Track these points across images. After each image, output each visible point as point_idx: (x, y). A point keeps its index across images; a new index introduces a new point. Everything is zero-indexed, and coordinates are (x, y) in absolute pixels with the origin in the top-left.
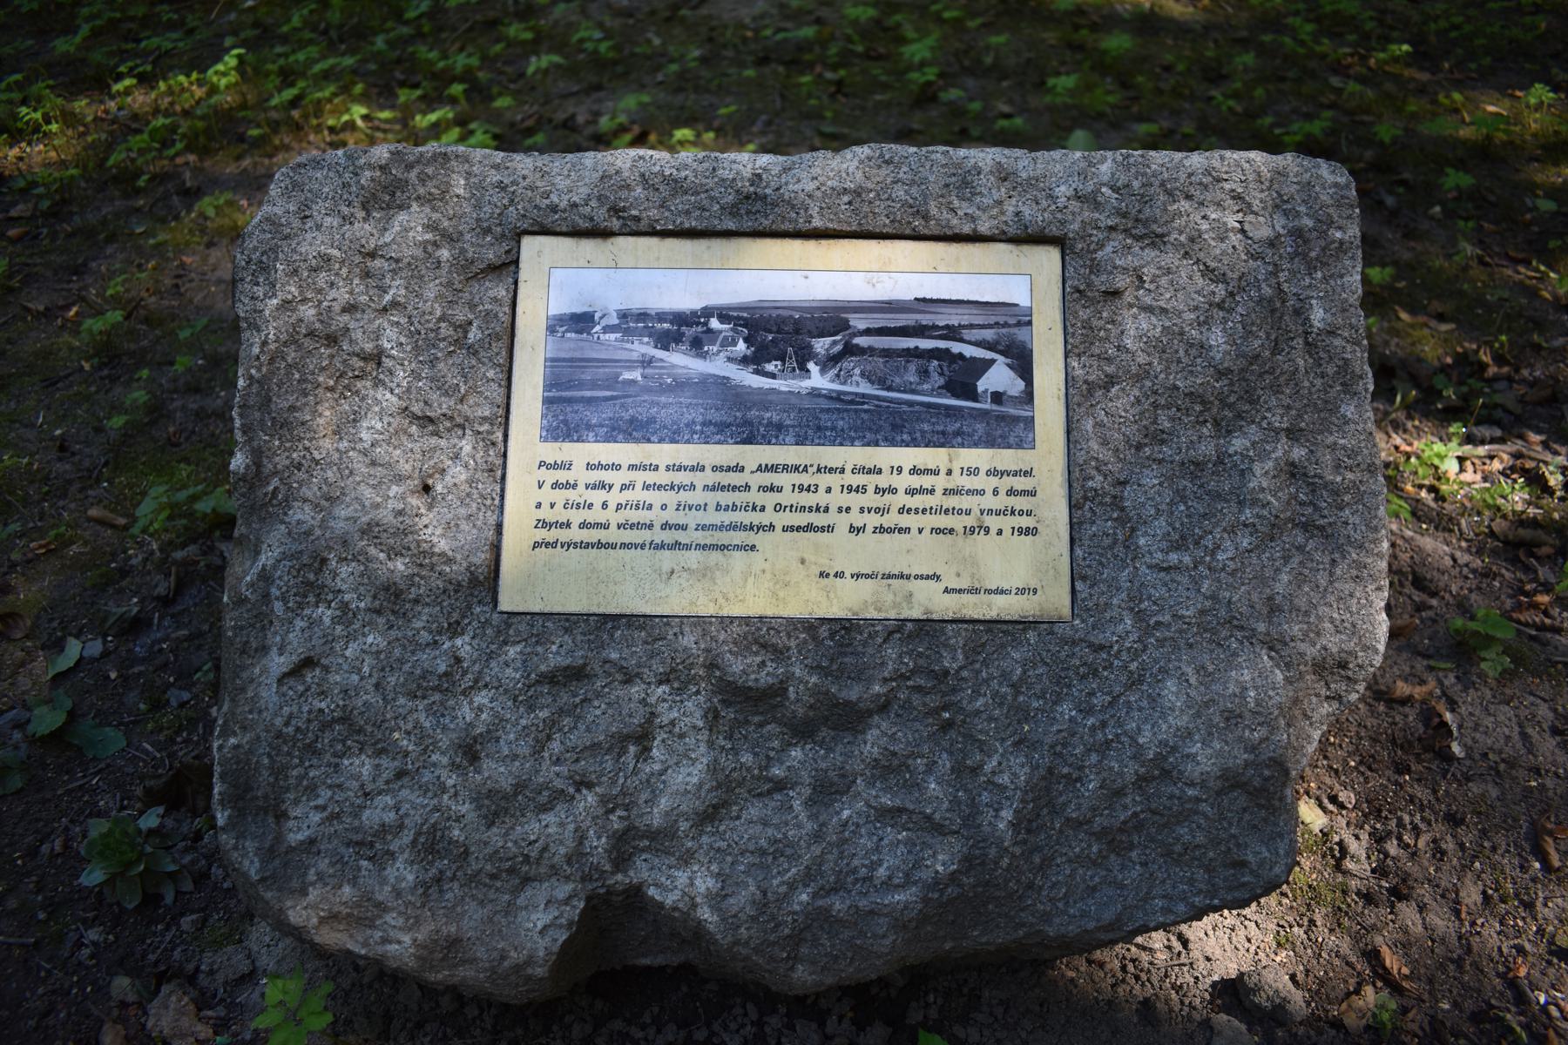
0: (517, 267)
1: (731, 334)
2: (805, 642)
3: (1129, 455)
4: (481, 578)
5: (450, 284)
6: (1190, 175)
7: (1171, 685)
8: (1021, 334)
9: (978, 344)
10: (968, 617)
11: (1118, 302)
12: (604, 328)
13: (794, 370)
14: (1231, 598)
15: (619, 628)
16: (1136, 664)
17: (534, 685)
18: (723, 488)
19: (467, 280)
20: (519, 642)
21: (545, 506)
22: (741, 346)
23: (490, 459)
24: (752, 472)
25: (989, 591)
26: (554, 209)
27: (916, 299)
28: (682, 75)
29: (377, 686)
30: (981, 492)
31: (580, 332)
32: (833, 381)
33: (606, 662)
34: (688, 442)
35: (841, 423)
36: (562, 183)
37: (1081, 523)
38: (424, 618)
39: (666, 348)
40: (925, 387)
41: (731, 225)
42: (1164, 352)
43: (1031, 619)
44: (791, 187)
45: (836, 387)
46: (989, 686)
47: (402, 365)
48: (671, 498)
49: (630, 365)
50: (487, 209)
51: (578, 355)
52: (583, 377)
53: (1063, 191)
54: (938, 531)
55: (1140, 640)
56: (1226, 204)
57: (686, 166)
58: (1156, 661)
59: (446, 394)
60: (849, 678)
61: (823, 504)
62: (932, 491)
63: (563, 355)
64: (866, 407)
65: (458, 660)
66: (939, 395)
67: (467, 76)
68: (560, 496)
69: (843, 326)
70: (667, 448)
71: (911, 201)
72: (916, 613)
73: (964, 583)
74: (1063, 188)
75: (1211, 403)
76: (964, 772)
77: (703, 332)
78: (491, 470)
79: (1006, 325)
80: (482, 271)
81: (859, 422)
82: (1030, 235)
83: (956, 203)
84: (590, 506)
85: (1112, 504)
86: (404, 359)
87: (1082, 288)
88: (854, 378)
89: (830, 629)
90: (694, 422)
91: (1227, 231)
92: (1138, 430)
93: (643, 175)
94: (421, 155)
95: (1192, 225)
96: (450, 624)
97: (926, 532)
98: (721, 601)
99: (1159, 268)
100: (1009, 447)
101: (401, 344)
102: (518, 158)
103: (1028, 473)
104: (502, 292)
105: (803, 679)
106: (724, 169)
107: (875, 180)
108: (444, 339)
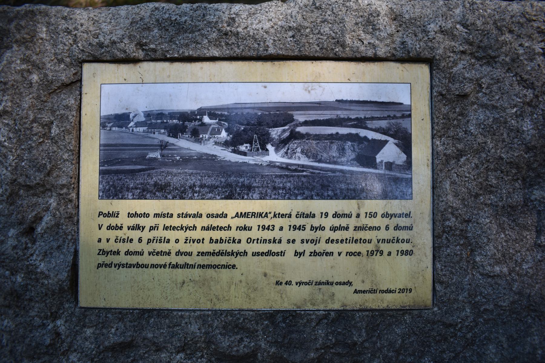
0: (81, 84)
1: (217, 126)
2: (267, 326)
3: (471, 201)
4: (66, 288)
5: (38, 97)
6: (512, 17)
7: (492, 348)
8: (404, 123)
9: (376, 130)
10: (369, 308)
11: (466, 101)
12: (136, 124)
13: (258, 149)
14: (530, 293)
15: (152, 317)
16: (470, 334)
17: (103, 352)
18: (214, 228)
19: (50, 94)
20: (92, 327)
21: (104, 241)
22: (224, 134)
23: (69, 211)
24: (232, 218)
25: (382, 292)
26: (101, 45)
27: (337, 101)
29: (11, 351)
30: (378, 228)
31: (120, 127)
32: (284, 157)
33: (144, 339)
34: (191, 198)
35: (289, 184)
36: (106, 28)
37: (440, 247)
38: (36, 310)
39: (175, 136)
40: (343, 159)
41: (216, 53)
42: (494, 135)
43: (408, 308)
44: (254, 26)
45: (286, 160)
46: (381, 352)
47: (11, 152)
48: (181, 235)
49: (152, 148)
50: (61, 46)
51: (120, 142)
52: (124, 156)
53: (432, 27)
54: (350, 254)
55: (474, 320)
56: (534, 37)
57: (185, 14)
58: (483, 333)
59: (39, 170)
60: (295, 347)
61: (277, 238)
62: (347, 228)
63: (111, 142)
64: (304, 173)
65: (58, 334)
66: (352, 165)
68: (112, 234)
69: (289, 120)
70: (178, 202)
71: (334, 35)
72: (336, 306)
73: (367, 287)
74: (432, 26)
75: (522, 168)
77: (199, 125)
78: (70, 217)
79: (395, 117)
80: (59, 88)
81: (300, 184)
82: (411, 57)
83: (363, 36)
84: (131, 241)
85: (460, 235)
86: (13, 148)
87: (444, 93)
88: (297, 154)
89: (283, 316)
90: (194, 185)
91: (535, 54)
92: (476, 185)
93: (157, 20)
94: (18, 12)
95: (513, 50)
96: (52, 313)
97: (343, 254)
98: (215, 300)
99: (492, 79)
100: (396, 198)
101: (10, 138)
102: (78, 12)
103: (408, 215)
104: (72, 102)
106: (210, 15)
107: (309, 21)
108: (36, 134)
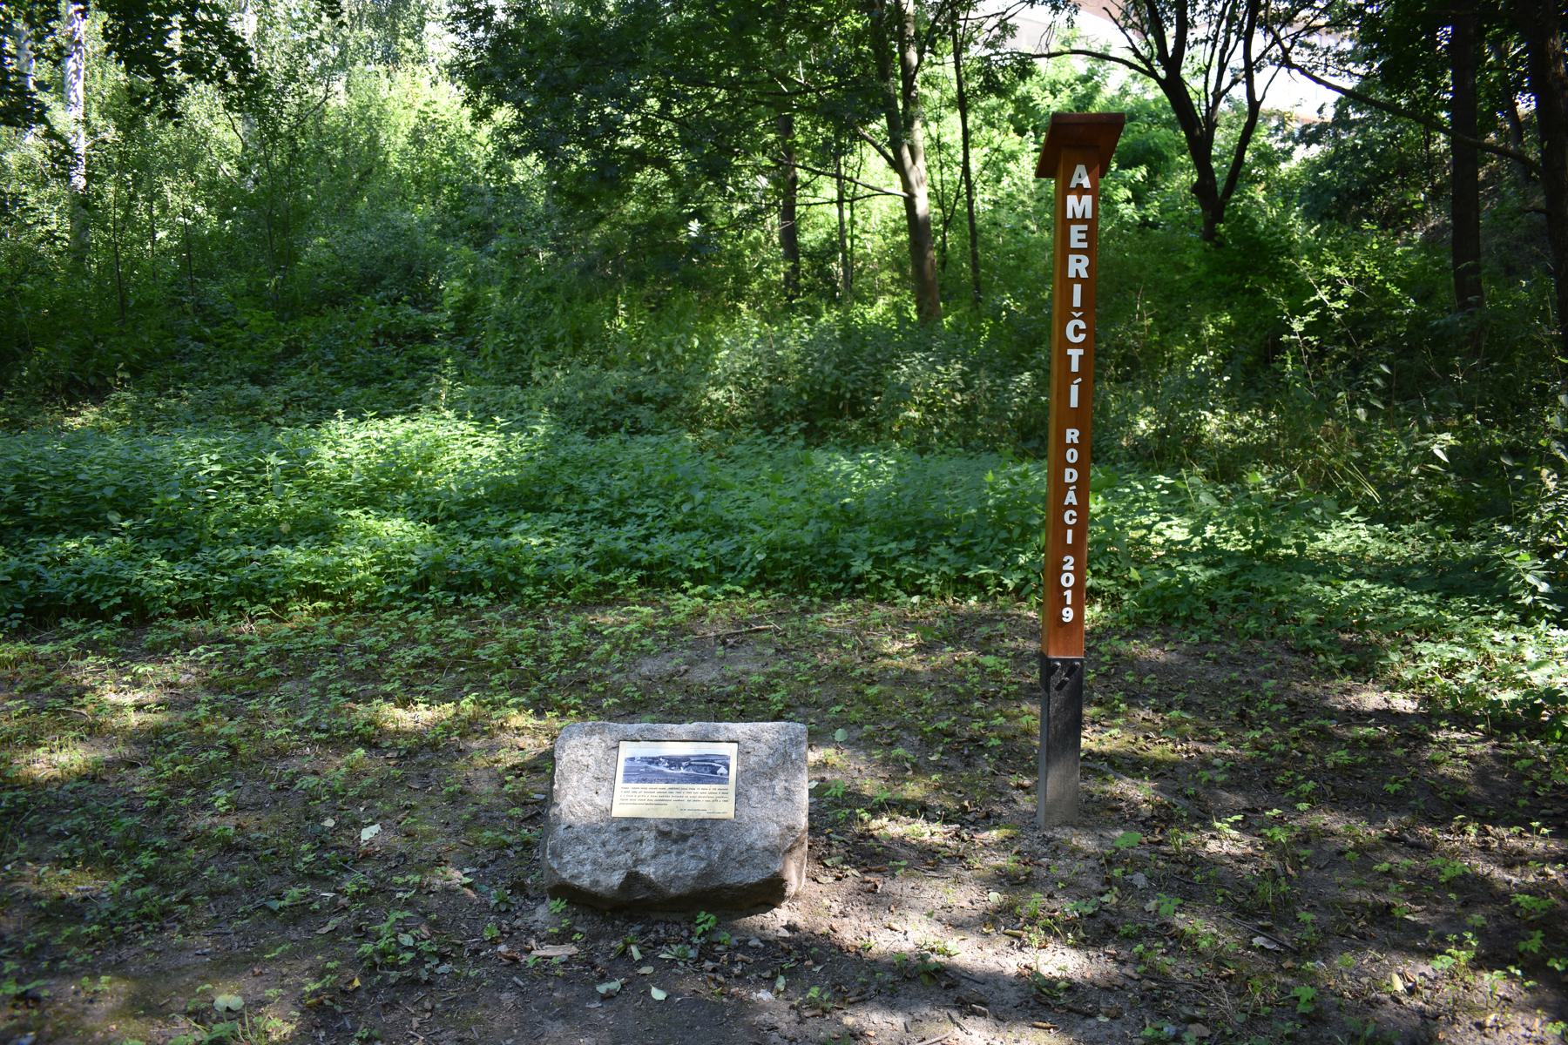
28: (672, 708)
67: (575, 707)
76: (709, 848)
105: (675, 830)
